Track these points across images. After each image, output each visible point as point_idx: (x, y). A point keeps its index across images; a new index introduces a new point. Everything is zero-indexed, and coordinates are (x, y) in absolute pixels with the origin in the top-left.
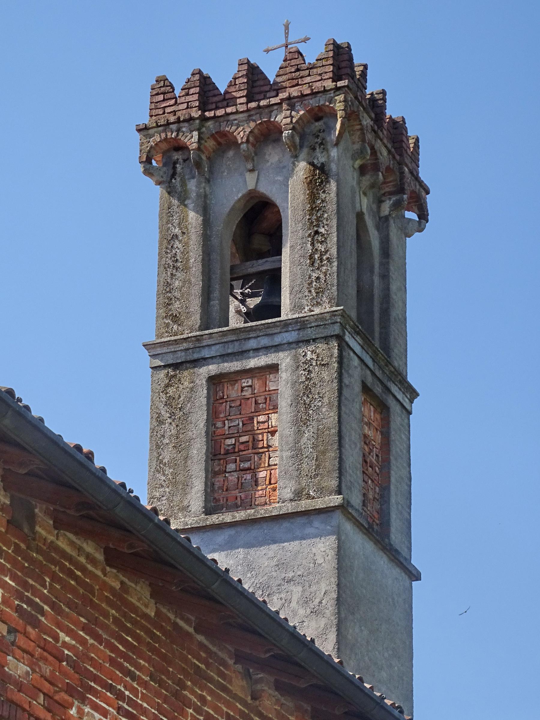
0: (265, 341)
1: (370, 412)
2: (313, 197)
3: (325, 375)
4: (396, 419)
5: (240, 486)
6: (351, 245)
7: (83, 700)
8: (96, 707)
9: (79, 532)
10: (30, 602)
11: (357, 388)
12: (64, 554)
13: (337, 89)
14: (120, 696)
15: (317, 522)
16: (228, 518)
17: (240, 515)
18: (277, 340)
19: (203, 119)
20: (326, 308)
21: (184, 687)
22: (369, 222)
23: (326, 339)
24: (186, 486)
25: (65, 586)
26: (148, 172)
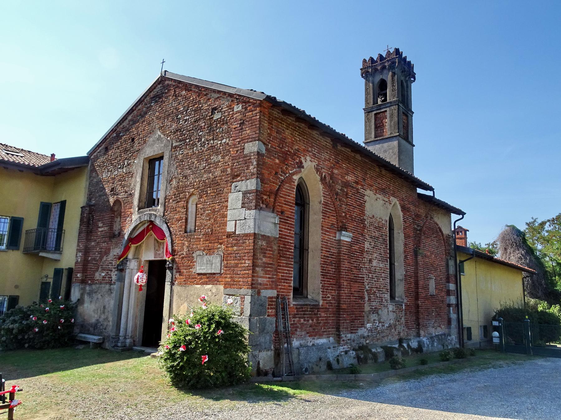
0: (384, 106)
1: (404, 117)
2: (392, 78)
3: (395, 111)
4: (410, 118)
5: (381, 133)
6: (400, 87)
7: (348, 175)
8: (350, 176)
9: (345, 147)
10: (337, 160)
11: (402, 113)
12: (343, 151)
13: (396, 57)
14: (355, 174)
15: (395, 139)
16: (378, 139)
17: (381, 138)
18: (387, 106)
19: (372, 66)
20: (395, 99)
21: (367, 171)
22: (404, 81)
23: (396, 105)
24: (371, 134)
25: (344, 156)
26: (363, 77)
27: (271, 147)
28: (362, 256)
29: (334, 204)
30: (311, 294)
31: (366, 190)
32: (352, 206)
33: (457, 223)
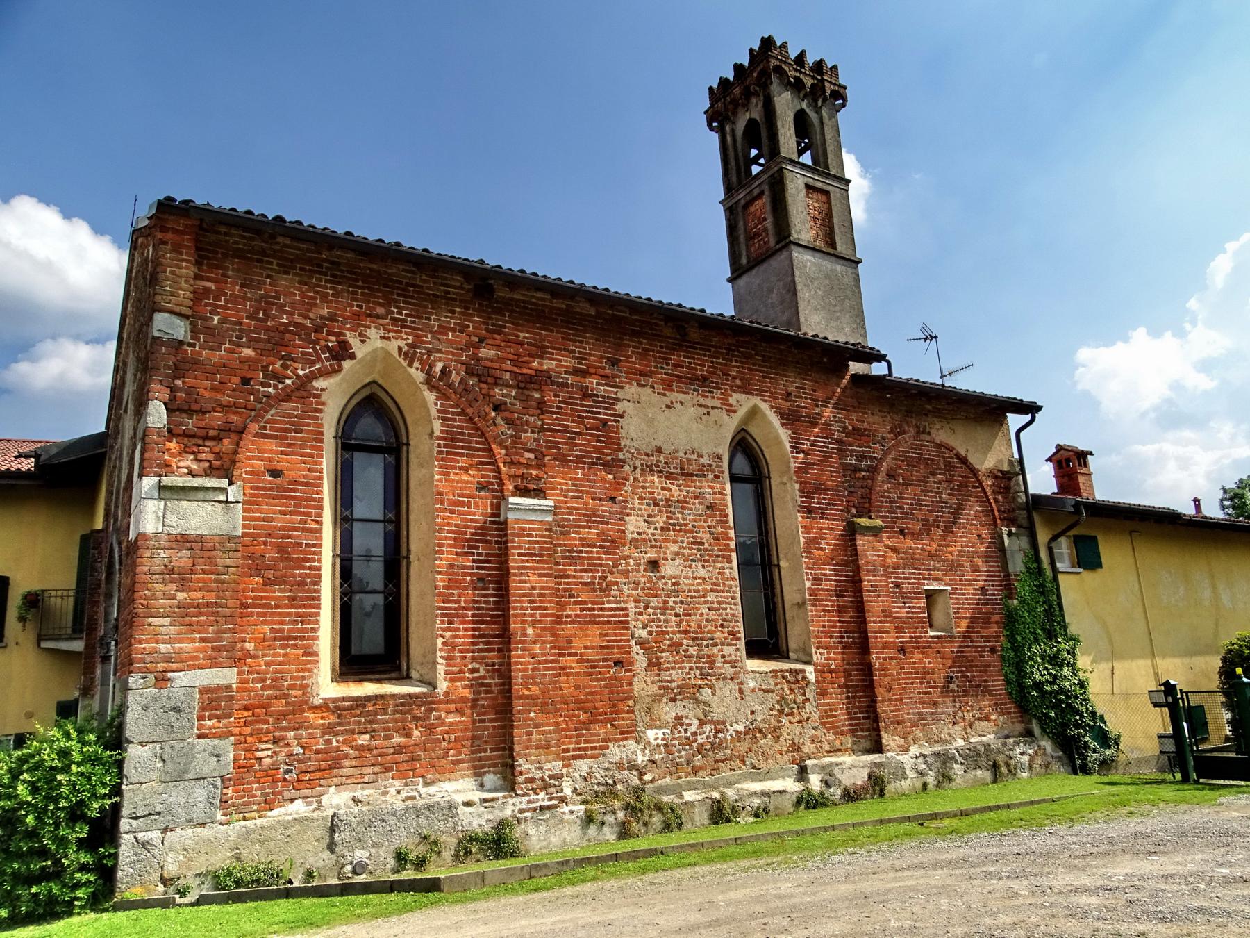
26: (711, 129)
27: (221, 321)
28: (615, 554)
29: (483, 435)
30: (418, 668)
31: (622, 388)
32: (567, 432)
33: (1022, 434)
